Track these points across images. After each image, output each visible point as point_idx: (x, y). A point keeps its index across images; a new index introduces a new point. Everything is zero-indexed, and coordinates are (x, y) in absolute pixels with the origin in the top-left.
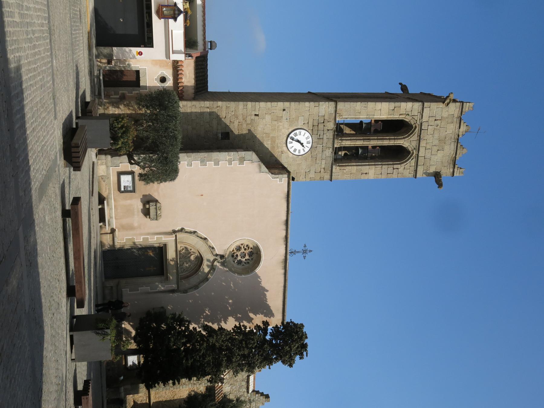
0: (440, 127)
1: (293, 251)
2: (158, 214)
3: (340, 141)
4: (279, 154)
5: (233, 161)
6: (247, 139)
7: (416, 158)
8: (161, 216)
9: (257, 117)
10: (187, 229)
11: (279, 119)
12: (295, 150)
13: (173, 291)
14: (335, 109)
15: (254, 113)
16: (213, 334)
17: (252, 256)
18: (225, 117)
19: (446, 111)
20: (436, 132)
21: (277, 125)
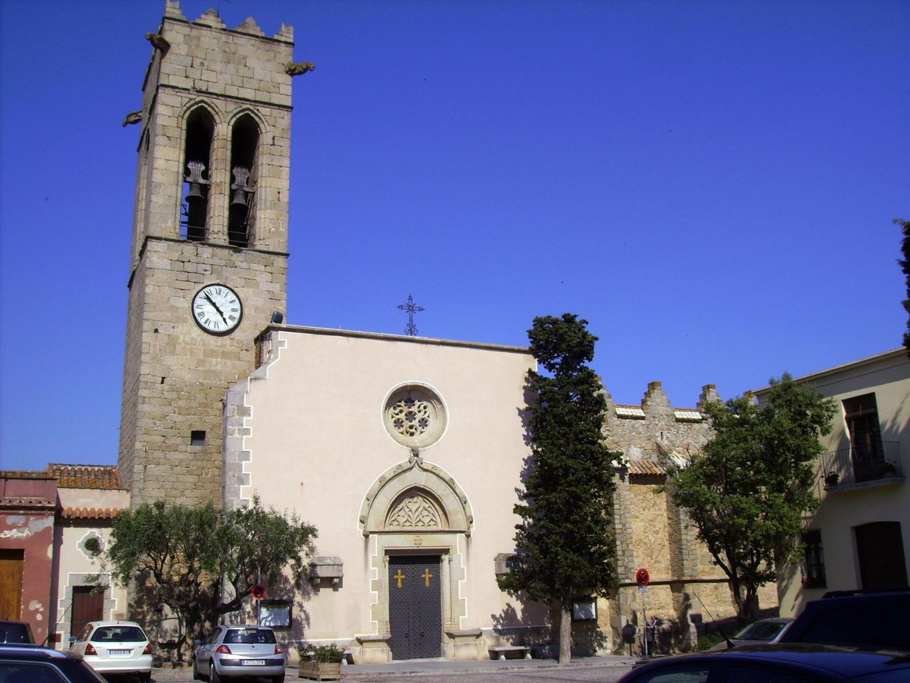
4: (235, 344)
11: (172, 342)
19: (177, 48)
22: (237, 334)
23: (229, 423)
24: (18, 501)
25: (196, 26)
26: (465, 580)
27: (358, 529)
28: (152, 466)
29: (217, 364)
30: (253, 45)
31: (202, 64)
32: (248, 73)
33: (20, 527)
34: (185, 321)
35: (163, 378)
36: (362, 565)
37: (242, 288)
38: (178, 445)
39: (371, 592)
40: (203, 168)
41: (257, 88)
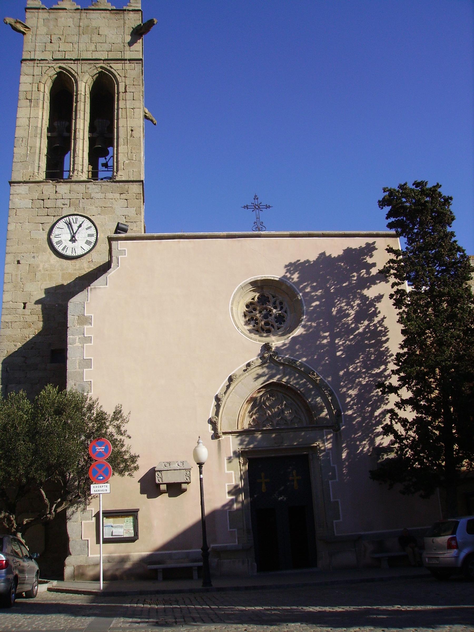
0: (63, 35)
2: (179, 468)
3: (76, 172)
5: (84, 334)
7: (109, 62)
8: (183, 463)
10: (211, 413)
11: (33, 270)
12: (88, 242)
14: (21, 184)
16: (350, 327)
17: (268, 298)
20: (69, 40)
21: (43, 272)
25: (53, 11)
26: (337, 480)
28: (13, 385)
30: (104, 18)
32: (102, 39)
35: (25, 304)
37: (99, 216)
41: (109, 50)
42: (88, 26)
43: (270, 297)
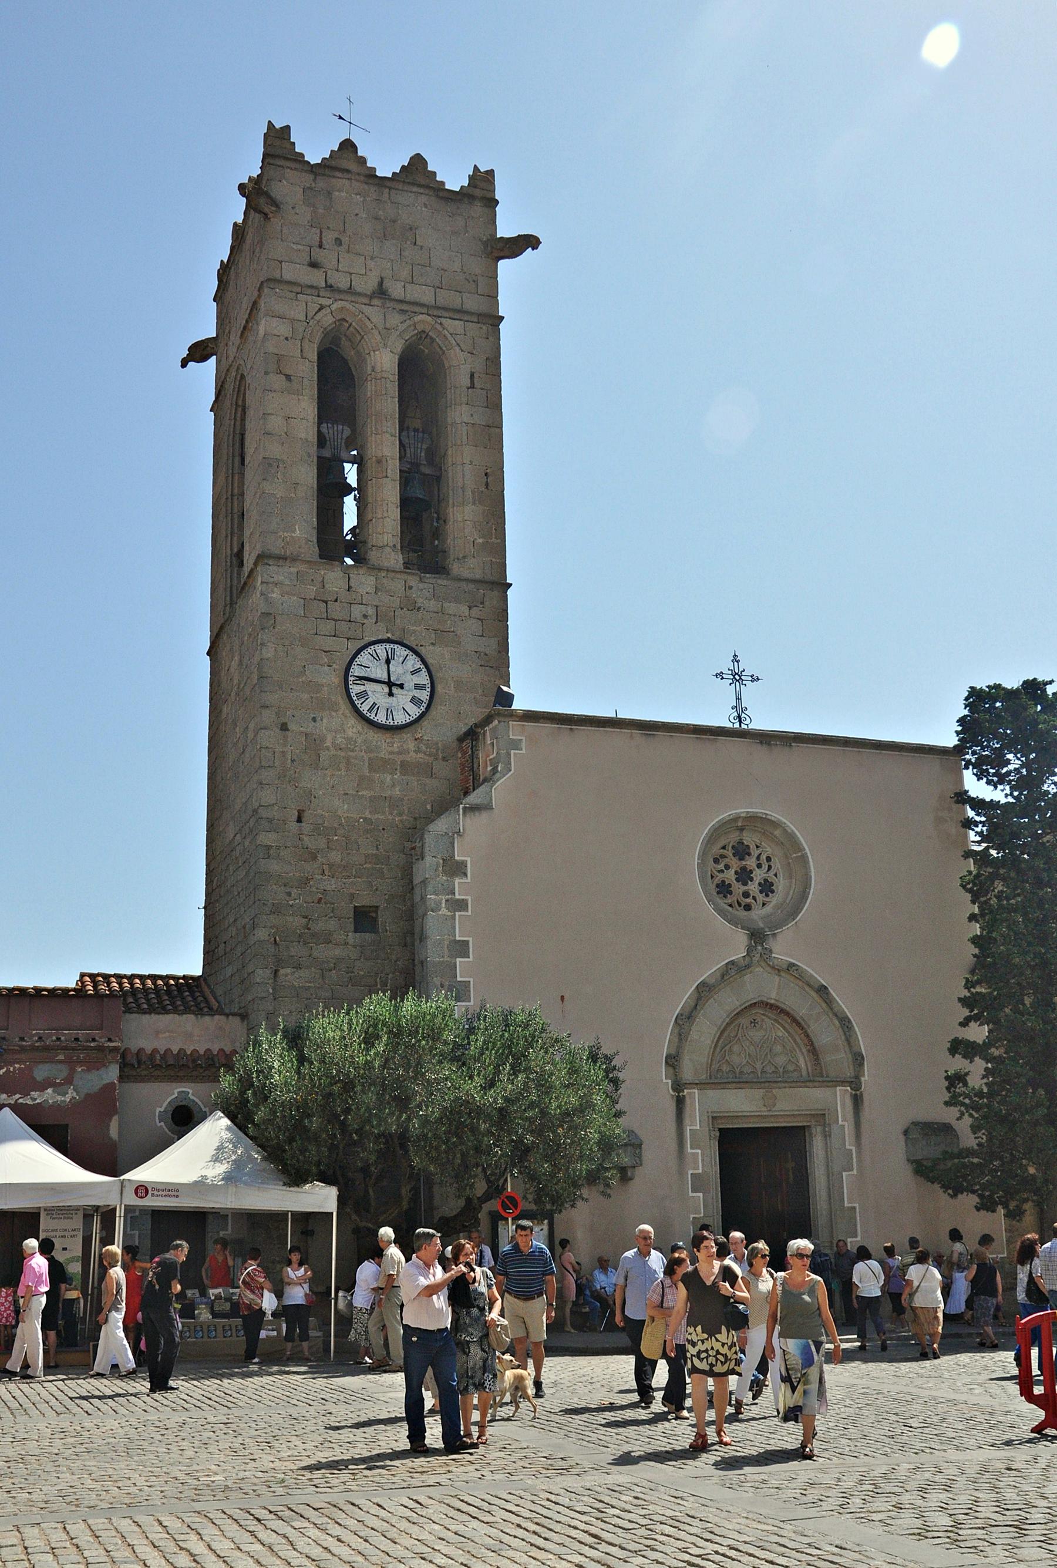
1: (736, 714)
6: (377, 849)
9: (306, 816)
11: (314, 744)
12: (415, 701)
13: (857, 1101)
15: (293, 826)
18: (305, 917)
19: (293, 212)
22: (426, 730)
23: (430, 888)
24: (54, 1038)
27: (664, 1081)
28: (289, 970)
29: (393, 786)
30: (425, 205)
31: (338, 242)
33: (60, 1084)
34: (333, 708)
36: (673, 1145)
37: (431, 647)
38: (331, 933)
39: (691, 1194)
40: (347, 432)
41: (438, 284)
42: (394, 221)
43: (752, 846)
